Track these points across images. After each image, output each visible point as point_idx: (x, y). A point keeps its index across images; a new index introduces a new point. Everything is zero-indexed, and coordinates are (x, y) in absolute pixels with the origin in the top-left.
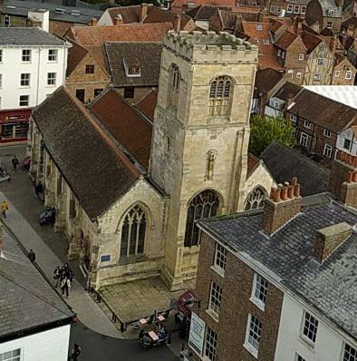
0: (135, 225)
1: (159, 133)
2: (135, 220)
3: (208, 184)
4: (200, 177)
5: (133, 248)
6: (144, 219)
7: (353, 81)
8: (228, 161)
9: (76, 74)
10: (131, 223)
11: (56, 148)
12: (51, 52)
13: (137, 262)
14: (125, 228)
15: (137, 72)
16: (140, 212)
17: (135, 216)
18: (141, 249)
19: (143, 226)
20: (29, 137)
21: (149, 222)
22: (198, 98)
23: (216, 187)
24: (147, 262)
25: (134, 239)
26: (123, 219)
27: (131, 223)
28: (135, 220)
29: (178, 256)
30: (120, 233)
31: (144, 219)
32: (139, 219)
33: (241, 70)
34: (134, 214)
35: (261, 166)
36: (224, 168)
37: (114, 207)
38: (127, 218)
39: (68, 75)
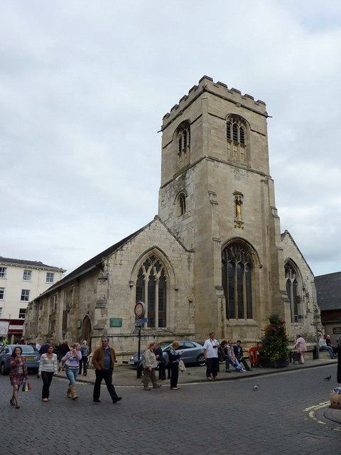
10: (147, 279)
16: (158, 266)
27: (147, 279)
28: (152, 277)
30: (135, 287)
32: (158, 275)
38: (141, 271)
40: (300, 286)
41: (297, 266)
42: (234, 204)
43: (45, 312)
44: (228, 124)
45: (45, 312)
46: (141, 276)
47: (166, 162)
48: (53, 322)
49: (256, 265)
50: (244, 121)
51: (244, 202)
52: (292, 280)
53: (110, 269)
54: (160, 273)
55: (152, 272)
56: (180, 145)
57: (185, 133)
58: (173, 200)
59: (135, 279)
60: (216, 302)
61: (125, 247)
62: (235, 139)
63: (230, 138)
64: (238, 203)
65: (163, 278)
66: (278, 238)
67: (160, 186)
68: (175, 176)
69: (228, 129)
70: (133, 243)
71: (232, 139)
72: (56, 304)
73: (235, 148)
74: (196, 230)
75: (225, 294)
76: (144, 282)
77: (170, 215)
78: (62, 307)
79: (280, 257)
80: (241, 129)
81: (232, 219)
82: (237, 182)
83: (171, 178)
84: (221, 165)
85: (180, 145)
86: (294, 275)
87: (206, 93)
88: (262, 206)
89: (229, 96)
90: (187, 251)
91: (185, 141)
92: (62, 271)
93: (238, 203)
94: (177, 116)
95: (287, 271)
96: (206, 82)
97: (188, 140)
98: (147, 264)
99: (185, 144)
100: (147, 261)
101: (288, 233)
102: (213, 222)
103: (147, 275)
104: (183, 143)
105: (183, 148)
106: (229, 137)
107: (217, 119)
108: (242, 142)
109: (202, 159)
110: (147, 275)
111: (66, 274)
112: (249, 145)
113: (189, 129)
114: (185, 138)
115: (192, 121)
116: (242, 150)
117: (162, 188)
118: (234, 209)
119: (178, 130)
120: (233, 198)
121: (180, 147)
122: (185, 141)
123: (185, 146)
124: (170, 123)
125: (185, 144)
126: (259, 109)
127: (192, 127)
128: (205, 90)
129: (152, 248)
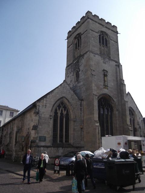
10: (59, 115)
16: (65, 108)
23: (111, 95)
27: (59, 115)
28: (62, 114)
38: (56, 110)
40: (136, 122)
41: (134, 112)
42: (103, 76)
43: (7, 132)
44: (100, 36)
45: (7, 132)
46: (56, 113)
47: (69, 54)
48: (11, 138)
49: (115, 109)
50: (107, 35)
51: (108, 76)
52: (132, 119)
53: (40, 108)
54: (66, 112)
55: (62, 111)
56: (76, 46)
57: (78, 40)
58: (72, 74)
59: (53, 114)
60: (96, 129)
61: (48, 97)
62: (103, 44)
63: (100, 43)
64: (105, 75)
65: (67, 114)
66: (125, 95)
67: (66, 66)
68: (73, 61)
69: (100, 38)
70: (52, 94)
71: (102, 43)
72: (12, 128)
73: (102, 48)
74: (84, 89)
75: (100, 125)
77: (71, 81)
78: (15, 129)
79: (126, 106)
80: (106, 39)
81: (102, 84)
82: (104, 65)
83: (71, 62)
84: (97, 56)
85: (76, 46)
86: (133, 116)
87: (89, 19)
88: (117, 78)
89: (100, 22)
90: (80, 100)
91: (79, 44)
92: (18, 111)
93: (105, 75)
94: (75, 31)
95: (130, 114)
96: (89, 14)
97: (80, 43)
98: (59, 106)
99: (79, 45)
100: (59, 105)
101: (129, 93)
102: (93, 85)
103: (59, 113)
104: (77, 45)
105: (77, 47)
106: (100, 42)
107: (94, 33)
108: (106, 45)
109: (87, 52)
110: (59, 113)
111: (19, 112)
112: (110, 47)
113: (81, 38)
114: (79, 42)
115: (82, 33)
116: (106, 49)
117: (67, 67)
118: (103, 79)
119: (75, 38)
120: (103, 73)
121: (76, 47)
122: (79, 44)
123: (79, 46)
124: (71, 35)
125: (79, 45)
126: (114, 29)
127: (82, 37)
128: (88, 18)
129: (62, 98)
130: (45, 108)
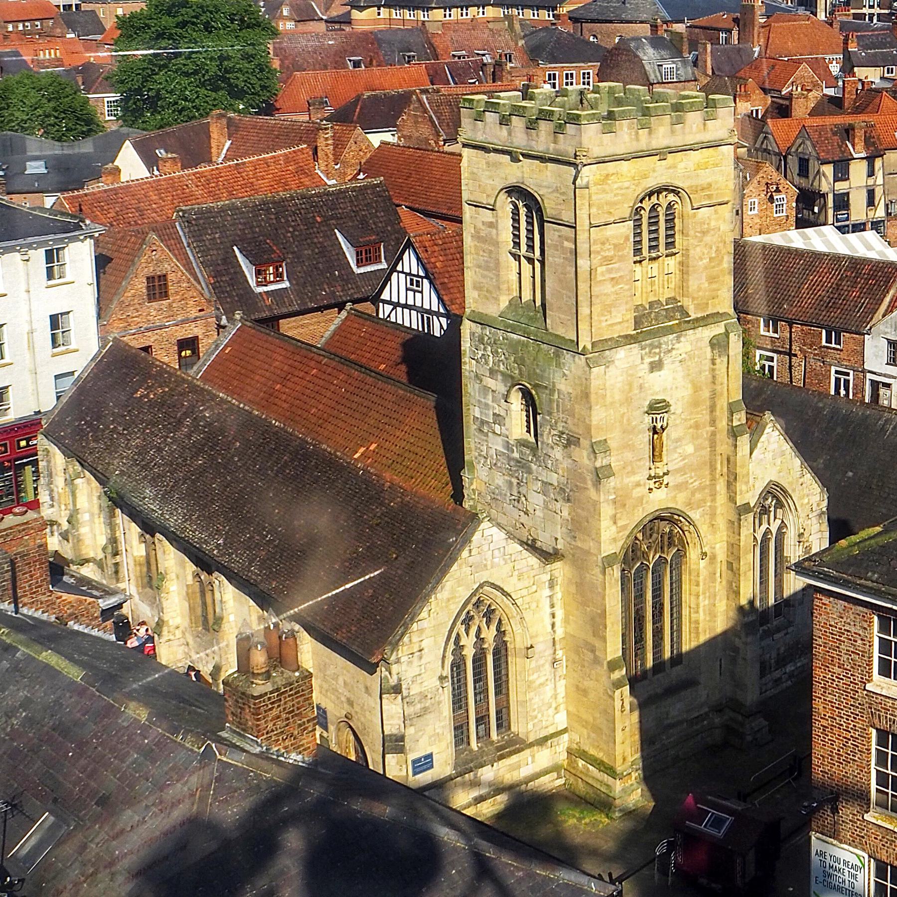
0: (479, 660)
1: (486, 389)
2: (480, 640)
3: (660, 500)
4: (638, 485)
5: (482, 719)
6: (501, 633)
7: (792, 220)
8: (697, 426)
9: (123, 306)
11: (165, 499)
12: (50, 256)
13: (501, 757)
14: (458, 666)
15: (278, 276)
16: (489, 615)
17: (479, 630)
18: (503, 722)
19: (501, 652)
20: (44, 497)
21: (516, 639)
22: (608, 260)
24: (527, 752)
25: (481, 693)
26: (451, 646)
27: (469, 652)
28: (480, 640)
29: (618, 713)
31: (501, 633)
32: (490, 634)
33: (699, 167)
34: (473, 630)
35: (768, 430)
36: (690, 449)
37: (424, 614)
39: (99, 317)
54: (493, 627)
76: (463, 659)
130: (421, 658)
